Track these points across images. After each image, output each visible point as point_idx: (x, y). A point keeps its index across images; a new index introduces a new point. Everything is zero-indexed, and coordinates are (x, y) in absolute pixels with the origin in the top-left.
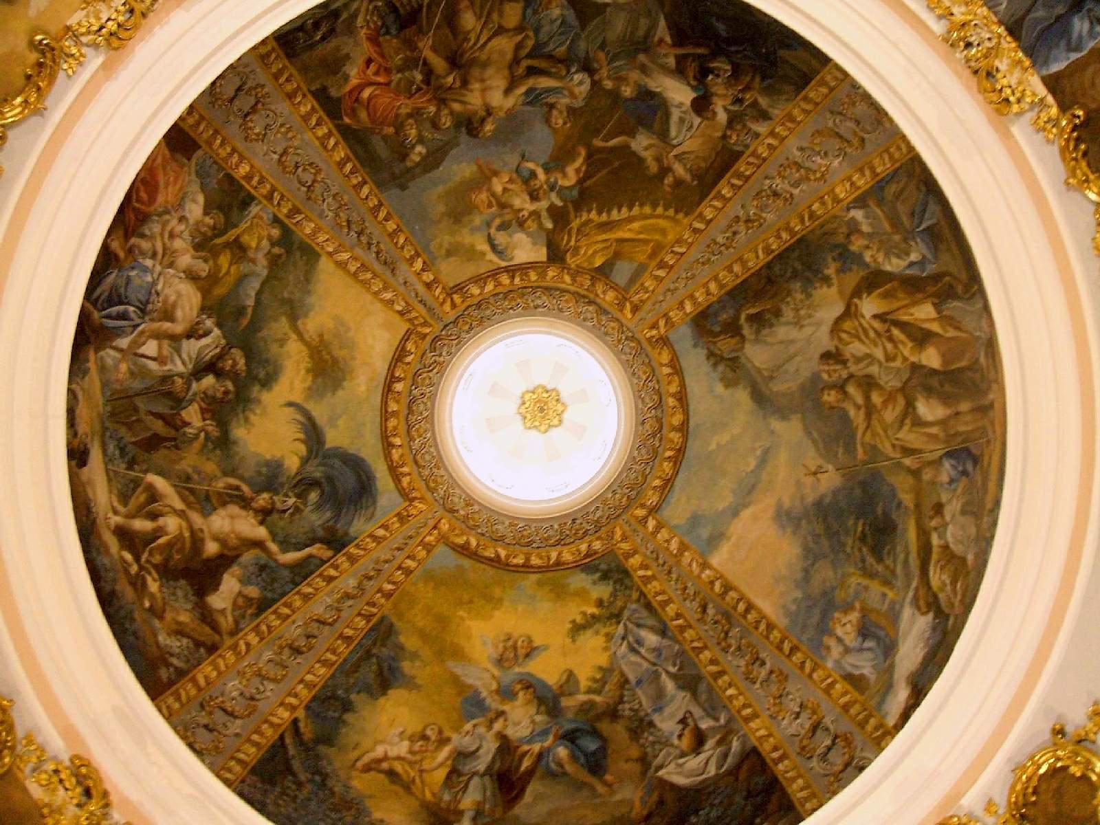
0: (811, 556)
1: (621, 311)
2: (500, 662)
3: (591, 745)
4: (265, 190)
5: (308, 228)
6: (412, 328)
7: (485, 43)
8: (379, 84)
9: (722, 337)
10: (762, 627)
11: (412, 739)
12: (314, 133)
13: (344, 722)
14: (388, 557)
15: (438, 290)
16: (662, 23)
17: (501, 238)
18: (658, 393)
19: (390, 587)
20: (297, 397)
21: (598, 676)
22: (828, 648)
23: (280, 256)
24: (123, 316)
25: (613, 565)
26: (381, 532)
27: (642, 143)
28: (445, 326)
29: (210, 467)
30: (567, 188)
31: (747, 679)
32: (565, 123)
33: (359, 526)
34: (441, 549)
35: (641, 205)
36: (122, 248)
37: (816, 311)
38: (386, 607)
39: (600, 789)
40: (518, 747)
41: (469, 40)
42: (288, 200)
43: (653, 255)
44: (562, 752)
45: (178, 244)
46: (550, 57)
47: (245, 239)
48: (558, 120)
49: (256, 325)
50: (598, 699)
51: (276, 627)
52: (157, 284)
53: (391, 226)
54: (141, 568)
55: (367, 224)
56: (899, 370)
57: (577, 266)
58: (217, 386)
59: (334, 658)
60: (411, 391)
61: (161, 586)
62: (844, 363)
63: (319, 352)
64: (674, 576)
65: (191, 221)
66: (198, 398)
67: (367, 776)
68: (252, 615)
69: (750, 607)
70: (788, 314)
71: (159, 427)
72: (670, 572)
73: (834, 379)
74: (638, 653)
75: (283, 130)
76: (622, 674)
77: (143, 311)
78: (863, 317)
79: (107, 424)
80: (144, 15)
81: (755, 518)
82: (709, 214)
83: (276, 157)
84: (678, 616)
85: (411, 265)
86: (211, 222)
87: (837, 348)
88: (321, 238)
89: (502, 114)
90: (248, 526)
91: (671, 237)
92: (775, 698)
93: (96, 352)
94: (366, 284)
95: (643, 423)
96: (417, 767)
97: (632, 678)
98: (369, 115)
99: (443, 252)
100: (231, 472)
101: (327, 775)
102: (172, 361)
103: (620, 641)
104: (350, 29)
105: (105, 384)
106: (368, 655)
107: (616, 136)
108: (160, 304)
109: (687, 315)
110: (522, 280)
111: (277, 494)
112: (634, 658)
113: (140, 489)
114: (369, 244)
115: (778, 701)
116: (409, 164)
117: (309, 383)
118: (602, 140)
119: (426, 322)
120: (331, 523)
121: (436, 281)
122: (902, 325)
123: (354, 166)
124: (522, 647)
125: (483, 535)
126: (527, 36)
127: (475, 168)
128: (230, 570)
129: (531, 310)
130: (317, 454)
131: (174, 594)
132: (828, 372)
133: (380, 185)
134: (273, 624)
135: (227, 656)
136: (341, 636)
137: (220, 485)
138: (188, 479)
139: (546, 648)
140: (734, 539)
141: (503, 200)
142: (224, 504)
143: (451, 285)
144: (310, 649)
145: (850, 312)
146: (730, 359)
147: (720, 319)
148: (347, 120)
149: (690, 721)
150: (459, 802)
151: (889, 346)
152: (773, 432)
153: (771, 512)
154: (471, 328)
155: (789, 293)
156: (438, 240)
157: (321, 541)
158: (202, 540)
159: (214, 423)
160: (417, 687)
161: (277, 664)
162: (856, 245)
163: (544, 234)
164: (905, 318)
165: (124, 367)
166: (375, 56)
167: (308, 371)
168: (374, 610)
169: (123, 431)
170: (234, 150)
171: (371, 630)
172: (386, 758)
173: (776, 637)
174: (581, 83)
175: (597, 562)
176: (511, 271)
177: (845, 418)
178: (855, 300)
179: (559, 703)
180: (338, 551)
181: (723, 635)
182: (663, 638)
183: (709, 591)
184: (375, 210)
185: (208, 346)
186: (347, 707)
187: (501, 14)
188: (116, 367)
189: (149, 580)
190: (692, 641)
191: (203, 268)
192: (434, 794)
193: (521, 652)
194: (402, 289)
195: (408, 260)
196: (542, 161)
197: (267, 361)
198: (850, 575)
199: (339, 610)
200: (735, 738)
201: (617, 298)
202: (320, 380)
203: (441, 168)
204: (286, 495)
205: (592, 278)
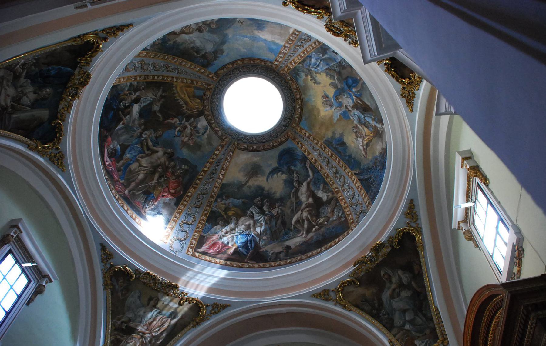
2: (331, 106)
3: (350, 81)
12: (188, 201)
14: (306, 142)
16: (118, 128)
17: (201, 131)
18: (233, 70)
23: (226, 196)
27: (156, 108)
28: (233, 138)
29: (289, 203)
30: (179, 120)
35: (176, 97)
40: (355, 103)
42: (209, 200)
44: (354, 90)
46: (142, 147)
47: (223, 209)
48: (160, 133)
50: (336, 78)
53: (208, 165)
54: (317, 225)
60: (256, 143)
70: (192, 45)
72: (290, 56)
76: (327, 69)
83: (198, 209)
85: (218, 154)
89: (164, 149)
90: (304, 188)
91: (182, 85)
93: (261, 248)
95: (245, 72)
97: (326, 67)
101: (368, 167)
102: (261, 221)
105: (269, 243)
106: (335, 148)
107: (158, 116)
110: (212, 120)
111: (294, 180)
112: (321, 66)
114: (216, 169)
118: (160, 118)
119: (234, 144)
121: (220, 145)
124: (325, 99)
126: (139, 158)
132: (205, 30)
133: (197, 173)
137: (293, 199)
138: (292, 210)
140: (273, 39)
144: (336, 168)
157: (305, 164)
158: (309, 204)
160: (342, 133)
165: (264, 237)
166: (161, 196)
167: (257, 177)
168: (322, 145)
169: (281, 234)
171: (328, 147)
172: (363, 146)
174: (146, 134)
175: (294, 77)
176: (210, 124)
178: (177, 33)
179: (339, 88)
180: (307, 159)
184: (205, 172)
186: (350, 156)
187: (136, 169)
189: (320, 222)
190: (311, 49)
192: (371, 133)
193: (327, 99)
203: (187, 158)
204: (294, 177)
205: (204, 100)
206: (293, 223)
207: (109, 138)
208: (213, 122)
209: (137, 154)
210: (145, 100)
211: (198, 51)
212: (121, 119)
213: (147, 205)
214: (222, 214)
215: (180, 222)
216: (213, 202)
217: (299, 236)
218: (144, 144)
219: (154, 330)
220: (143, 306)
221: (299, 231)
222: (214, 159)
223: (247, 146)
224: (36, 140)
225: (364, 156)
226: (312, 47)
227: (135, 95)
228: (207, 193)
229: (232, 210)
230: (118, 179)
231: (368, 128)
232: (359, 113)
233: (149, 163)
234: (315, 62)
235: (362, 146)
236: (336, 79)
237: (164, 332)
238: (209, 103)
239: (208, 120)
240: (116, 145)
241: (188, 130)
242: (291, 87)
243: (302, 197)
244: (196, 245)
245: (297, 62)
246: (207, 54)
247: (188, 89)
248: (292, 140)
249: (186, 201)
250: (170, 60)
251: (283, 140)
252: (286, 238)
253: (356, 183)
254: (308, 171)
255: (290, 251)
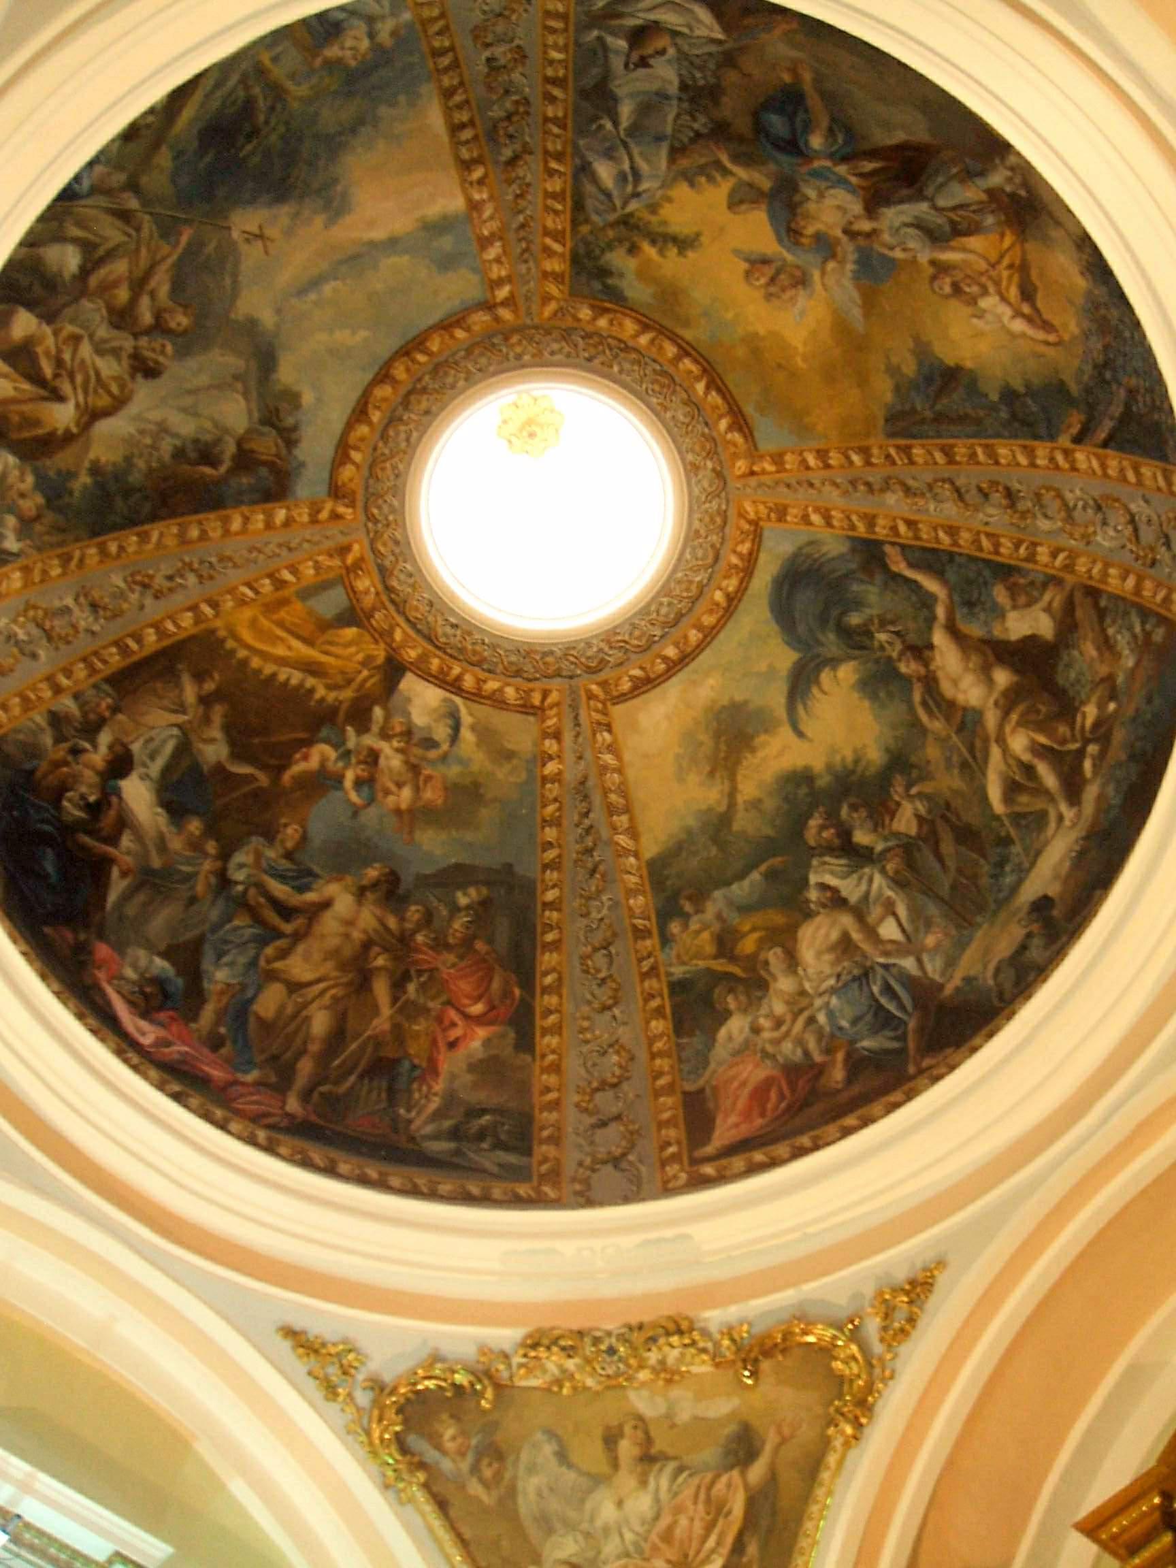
0: (334, 144)
1: (362, 559)
2: (802, 281)
3: (777, 123)
4: (652, 984)
5: (638, 902)
6: (609, 704)
7: (319, 981)
8: (458, 1010)
9: (264, 457)
10: (458, 98)
11: (973, 301)
12: (560, 1004)
13: (1028, 386)
14: (828, 488)
15: (550, 723)
16: (112, 897)
17: (441, 732)
18: (384, 437)
19: (856, 458)
20: (786, 732)
21: (703, 179)
22: (394, 33)
23: (689, 898)
24: (888, 990)
25: (583, 278)
26: (816, 518)
28: (571, 677)
31: (525, 57)
32: (286, 825)
33: (833, 546)
34: (765, 446)
36: (833, 1062)
37: (132, 436)
38: (878, 445)
39: (807, 77)
40: (863, 188)
41: (334, 997)
43: (284, 602)
44: (816, 141)
45: (779, 1008)
46: (258, 920)
47: (710, 949)
48: (291, 833)
49: (767, 848)
50: (725, 159)
51: (1011, 538)
52: (832, 987)
53: (550, 834)
54: (1087, 742)
55: (574, 855)
56: (72, 321)
57: (376, 642)
58: (858, 823)
59: (979, 451)
60: (662, 637)
61: (1083, 703)
62: (136, 356)
63: (726, 759)
64: (521, 218)
65: (749, 1019)
66: (886, 832)
67: (1056, 322)
68: (1023, 577)
69: (455, 129)
70: (167, 446)
71: (948, 847)
72: (522, 226)
73: (160, 341)
74: (633, 168)
75: (589, 1036)
76: (672, 160)
77: (866, 975)
78: (77, 405)
79: (993, 906)
80: (641, 1327)
81: (371, 224)
82: (187, 620)
83: (616, 1011)
84: (551, 173)
85: (560, 773)
86: (730, 999)
87: (133, 377)
88: (633, 880)
89: (349, 879)
91: (247, 613)
92: (508, 18)
93: (941, 987)
94: (623, 791)
95: (427, 412)
96: (993, 273)
98: (490, 981)
99: (515, 762)
100: (915, 724)
101: (1095, 366)
102: (880, 894)
103: (644, 195)
104: (450, 1099)
105: (961, 945)
106: (939, 418)
108: (846, 964)
109: (288, 508)
110: (451, 668)
111: (890, 658)
112: (643, 166)
113: (1017, 809)
114: (588, 830)
115: (507, 13)
116: (485, 891)
117: (763, 738)
118: (256, 779)
120: (860, 575)
121: (545, 735)
122: (37, 379)
123: (544, 933)
124: (763, 275)
125: (707, 424)
126: (268, 962)
127: (418, 835)
128: (1002, 636)
129: (465, 627)
130: (812, 659)
131: (1078, 681)
132: (163, 352)
133: (529, 888)
134: (1009, 545)
135: (1084, 569)
136: (951, 461)
137: (937, 726)
138: (964, 765)
139: (737, 252)
140: (418, 214)
141: (410, 775)
142: (952, 704)
143: (531, 719)
144: (998, 483)
145: (91, 416)
146: (273, 425)
147: (253, 481)
148: (517, 992)
149: (635, 57)
150: (981, 202)
151: (67, 356)
152: (278, 311)
153: (348, 220)
154: (545, 654)
155: (151, 470)
156: (512, 779)
157: (885, 567)
158: (1006, 694)
159: (892, 792)
160: (917, 339)
161: (1042, 506)
162: (31, 505)
163: (390, 705)
164: (26, 386)
165: (930, 940)
167: (753, 750)
168: (892, 451)
169: (985, 881)
170: (653, 1056)
171: (914, 437)
172: (1018, 314)
173: (452, 78)
174: (241, 866)
175: (600, 296)
176: (454, 686)
177: (177, 287)
178: (75, 430)
179: (771, 189)
180: (878, 544)
181: (515, 119)
182: (590, 164)
183: (491, 176)
184: (554, 865)
185: (832, 873)
186: (1009, 395)
187: (282, 1008)
188: (938, 946)
189: (1089, 722)
190: (558, 136)
191: (774, 956)
192: (1002, 235)
193: (769, 271)
194: (588, 755)
195: (559, 781)
196: (339, 794)
197: (786, 799)
198: (301, 99)
199: (930, 487)
200: (595, 8)
201: (357, 576)
202: (750, 730)
203: (453, 861)
205: (370, 616)
206: (998, 805)
207: (102, 950)
208: (456, 670)
209: (252, 953)
210: (152, 746)
211: (207, 455)
212: (109, 861)
213: (409, 1110)
214: (719, 968)
215: (576, 1098)
216: (658, 947)
217: (1053, 836)
218: (258, 903)
219: (698, 1552)
220: (598, 1480)
221: (1042, 816)
222: (556, 800)
223: (642, 668)
224: (458, 1388)
225: (1047, 343)
226: (555, 120)
227: (95, 747)
228: (615, 935)
229: (746, 928)
230: (229, 1077)
231: (974, 229)
232: (905, 207)
233: (325, 959)
234: (615, 172)
235: (1013, 317)
236: (729, 165)
237: (746, 1539)
238: (395, 614)
239: (436, 677)
240: (143, 962)
241: (387, 758)
242: (620, 341)
243: (965, 692)
244: (685, 1142)
245: (564, 231)
246: (247, 446)
247: (283, 614)
248: (778, 525)
249: (551, 1012)
250: (136, 553)
251: (745, 548)
252: (1008, 880)
253: (1104, 466)
254: (915, 582)
255: (1055, 913)
